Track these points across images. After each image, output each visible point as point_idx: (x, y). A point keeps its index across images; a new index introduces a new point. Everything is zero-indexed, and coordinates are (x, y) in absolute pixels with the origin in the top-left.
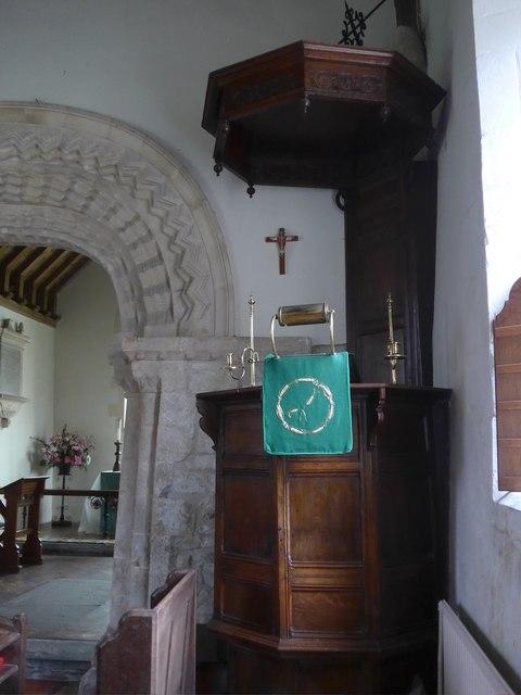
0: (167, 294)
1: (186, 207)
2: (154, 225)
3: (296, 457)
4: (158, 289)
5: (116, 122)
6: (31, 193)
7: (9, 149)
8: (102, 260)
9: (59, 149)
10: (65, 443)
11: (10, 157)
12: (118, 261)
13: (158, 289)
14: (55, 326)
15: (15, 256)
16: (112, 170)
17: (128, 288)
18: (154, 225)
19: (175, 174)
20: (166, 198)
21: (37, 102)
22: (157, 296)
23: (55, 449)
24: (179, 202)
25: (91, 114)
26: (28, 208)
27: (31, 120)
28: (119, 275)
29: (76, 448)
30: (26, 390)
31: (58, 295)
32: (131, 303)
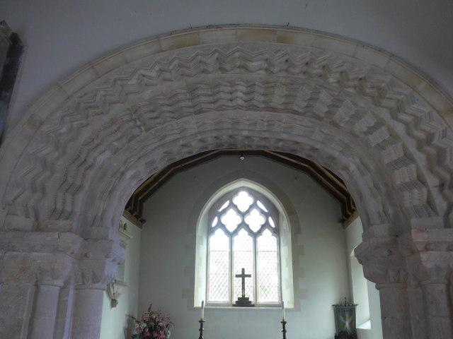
0: (425, 190)
1: (435, 114)
2: (399, 129)
3: (210, 309)
4: (409, 186)
5: (359, 43)
6: (277, 101)
7: (260, 63)
8: (344, 160)
9: (307, 64)
10: (154, 320)
11: (260, 69)
12: (357, 160)
13: (409, 186)
14: (141, 227)
15: (171, 165)
16: (356, 83)
17: (371, 185)
18: (399, 129)
19: (422, 86)
20: (415, 106)
21: (288, 26)
22: (416, 191)
23: (145, 325)
24: (427, 109)
25: (335, 36)
26: (267, 115)
27: (282, 40)
28: (362, 174)
29: (161, 324)
30: (126, 279)
31: (144, 204)
32: (380, 198)
